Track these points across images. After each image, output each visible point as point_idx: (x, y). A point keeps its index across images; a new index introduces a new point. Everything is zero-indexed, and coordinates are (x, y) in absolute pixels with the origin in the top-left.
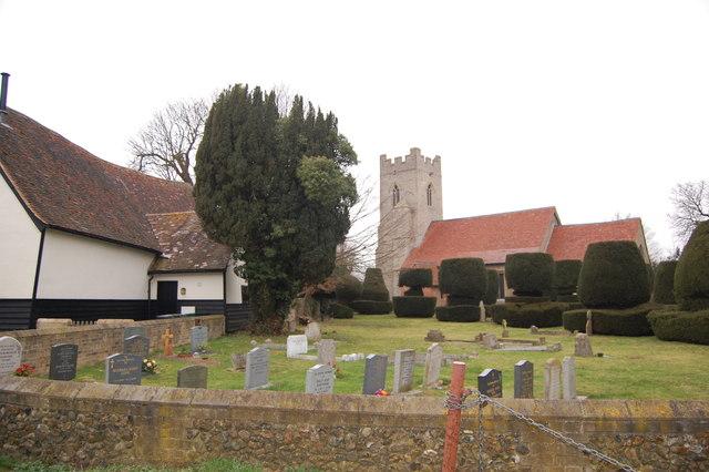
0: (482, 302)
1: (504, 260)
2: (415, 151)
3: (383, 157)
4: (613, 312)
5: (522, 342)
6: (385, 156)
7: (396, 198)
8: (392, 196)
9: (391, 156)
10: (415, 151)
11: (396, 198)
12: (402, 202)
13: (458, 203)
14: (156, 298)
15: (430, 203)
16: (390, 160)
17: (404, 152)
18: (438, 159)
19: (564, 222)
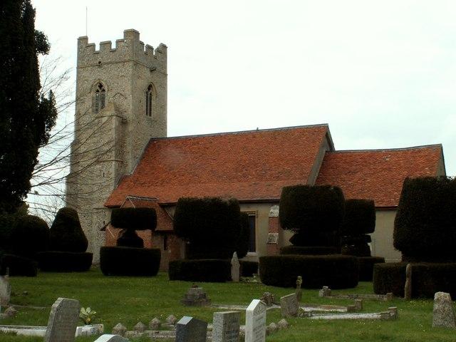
0: (235, 253)
1: (277, 195)
2: (132, 35)
3: (83, 41)
4: (312, 256)
5: (331, 312)
6: (85, 39)
7: (100, 103)
8: (94, 95)
9: (96, 40)
10: (132, 35)
11: (100, 103)
12: (109, 111)
13: (189, 113)
14: (241, 211)
15: (149, 111)
16: (93, 45)
17: (114, 35)
18: (163, 49)
19: (338, 146)
